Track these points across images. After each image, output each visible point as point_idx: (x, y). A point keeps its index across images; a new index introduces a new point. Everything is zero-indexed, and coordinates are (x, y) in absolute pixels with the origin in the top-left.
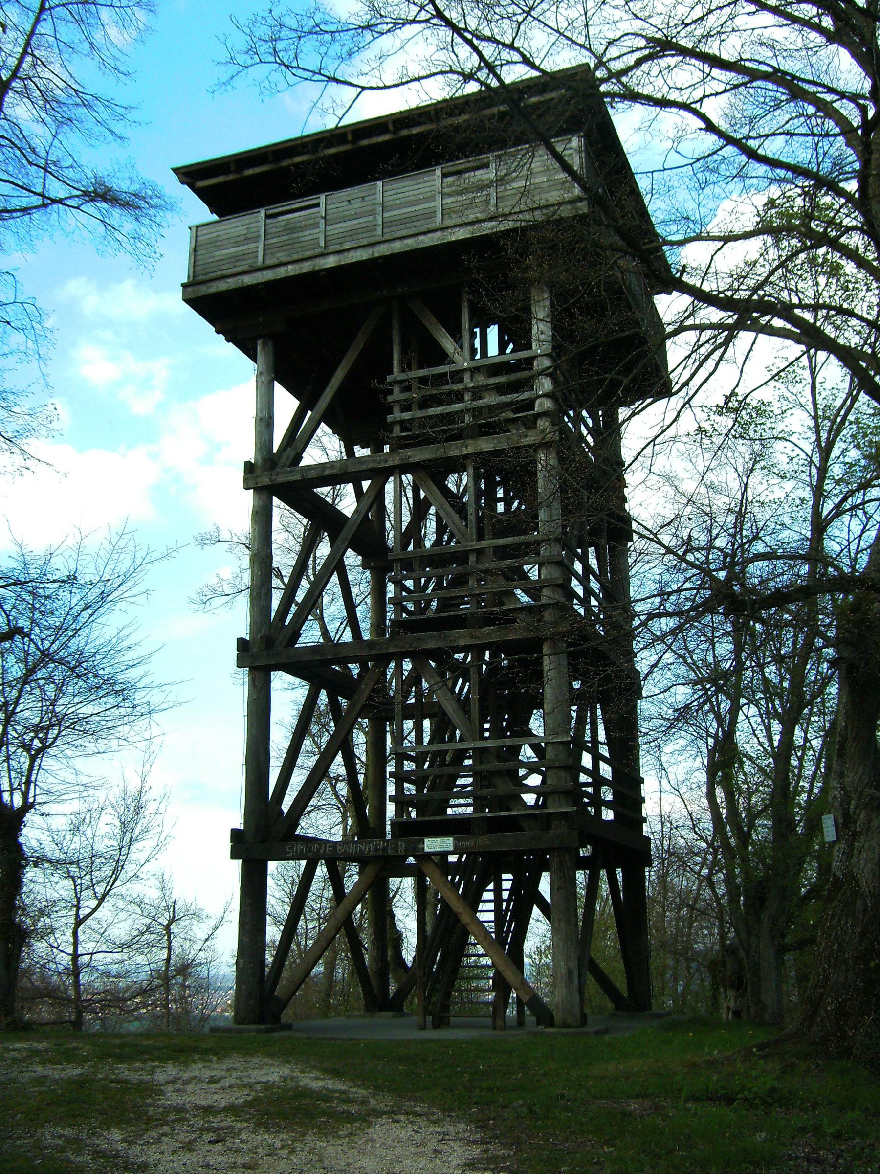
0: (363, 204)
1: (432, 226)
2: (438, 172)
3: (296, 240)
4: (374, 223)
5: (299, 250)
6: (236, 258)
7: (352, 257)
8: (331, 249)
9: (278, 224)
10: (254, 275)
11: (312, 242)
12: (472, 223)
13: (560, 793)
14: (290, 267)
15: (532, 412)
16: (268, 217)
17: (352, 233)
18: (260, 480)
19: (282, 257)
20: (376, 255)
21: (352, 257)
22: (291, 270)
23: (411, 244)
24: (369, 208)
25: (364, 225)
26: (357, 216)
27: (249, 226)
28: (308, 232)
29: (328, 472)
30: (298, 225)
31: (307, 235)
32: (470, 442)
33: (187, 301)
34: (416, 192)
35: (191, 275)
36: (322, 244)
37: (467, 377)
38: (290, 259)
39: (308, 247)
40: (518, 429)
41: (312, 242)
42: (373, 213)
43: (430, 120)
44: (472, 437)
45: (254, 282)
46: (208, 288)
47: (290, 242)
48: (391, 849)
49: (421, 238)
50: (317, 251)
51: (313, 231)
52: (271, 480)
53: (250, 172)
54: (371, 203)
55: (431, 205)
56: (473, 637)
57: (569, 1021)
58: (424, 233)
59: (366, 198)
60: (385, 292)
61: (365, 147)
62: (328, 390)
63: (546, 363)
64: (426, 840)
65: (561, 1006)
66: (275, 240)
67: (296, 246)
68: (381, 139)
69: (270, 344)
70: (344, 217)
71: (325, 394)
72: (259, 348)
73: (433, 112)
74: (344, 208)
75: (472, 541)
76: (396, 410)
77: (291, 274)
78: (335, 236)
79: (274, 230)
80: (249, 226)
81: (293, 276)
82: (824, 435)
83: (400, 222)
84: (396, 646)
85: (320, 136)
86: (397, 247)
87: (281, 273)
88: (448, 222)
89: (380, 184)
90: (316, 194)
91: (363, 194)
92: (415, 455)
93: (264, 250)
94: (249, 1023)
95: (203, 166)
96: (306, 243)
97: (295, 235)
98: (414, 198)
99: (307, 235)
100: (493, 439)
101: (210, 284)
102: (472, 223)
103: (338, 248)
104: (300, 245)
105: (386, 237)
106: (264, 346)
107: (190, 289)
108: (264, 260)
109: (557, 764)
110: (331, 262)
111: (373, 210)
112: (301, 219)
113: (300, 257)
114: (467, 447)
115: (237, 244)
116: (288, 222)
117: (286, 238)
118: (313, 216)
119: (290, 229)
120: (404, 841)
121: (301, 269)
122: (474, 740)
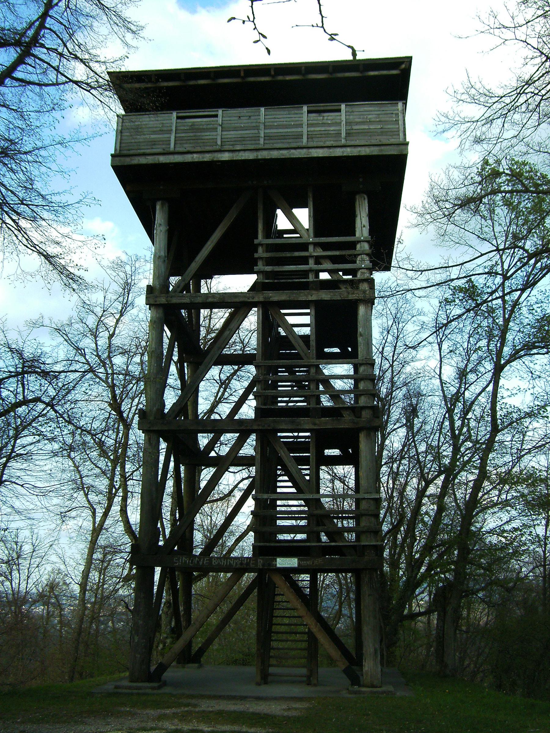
0: (250, 121)
1: (299, 144)
2: (305, 108)
3: (201, 137)
4: (257, 135)
5: (201, 144)
6: (154, 143)
7: (242, 156)
8: (226, 148)
9: (185, 124)
10: (167, 156)
11: (212, 141)
12: (329, 147)
13: (371, 532)
14: (195, 156)
15: (356, 278)
16: (178, 118)
17: (242, 140)
18: (158, 299)
19: (188, 147)
20: (260, 157)
21: (242, 156)
22: (196, 158)
23: (285, 154)
24: (254, 124)
25: (251, 135)
26: (242, 129)
27: (164, 122)
28: (208, 134)
29: (210, 300)
30: (201, 127)
31: (208, 135)
32: (314, 292)
33: (116, 168)
34: (288, 119)
35: (118, 148)
36: (219, 143)
37: (311, 248)
38: (195, 150)
39: (208, 144)
40: (346, 288)
41: (212, 141)
42: (257, 128)
43: (150, 81)
44: (316, 289)
45: (168, 161)
46: (131, 160)
47: (194, 138)
48: (253, 564)
49: (292, 151)
50: (215, 148)
51: (212, 133)
52: (167, 301)
53: (372, 73)
54: (255, 121)
55: (299, 130)
56: (315, 424)
57: (375, 683)
58: (295, 148)
59: (252, 118)
60: (255, 182)
61: (220, 84)
62: (209, 243)
63: (366, 246)
64: (278, 560)
65: (370, 673)
66: (183, 135)
67: (199, 141)
68: (263, 79)
69: (167, 205)
70: (235, 128)
71: (206, 246)
72: (158, 207)
73: (303, 68)
74: (236, 122)
75: (313, 359)
76: (260, 263)
77: (196, 160)
78: (229, 140)
79: (182, 128)
80: (164, 122)
81: (197, 162)
82: (507, 316)
83: (276, 138)
84: (259, 425)
85: (221, 69)
86: (275, 154)
87: (188, 158)
88: (311, 144)
89: (262, 109)
90: (170, 110)
91: (250, 114)
92: (274, 297)
93: (175, 140)
94: (142, 682)
95: (321, 65)
96: (206, 141)
97: (199, 134)
98: (287, 123)
99: (208, 135)
100: (330, 292)
101: (133, 158)
102: (329, 147)
103: (231, 148)
104: (202, 141)
105: (267, 146)
106: (162, 206)
107: (117, 159)
108: (175, 147)
109: (370, 513)
110: (226, 157)
111: (257, 126)
112: (203, 123)
113: (203, 149)
114: (311, 296)
115: (154, 133)
116: (193, 124)
117: (191, 134)
118: (213, 123)
119: (193, 128)
120: (262, 559)
121: (203, 158)
122: (312, 493)
